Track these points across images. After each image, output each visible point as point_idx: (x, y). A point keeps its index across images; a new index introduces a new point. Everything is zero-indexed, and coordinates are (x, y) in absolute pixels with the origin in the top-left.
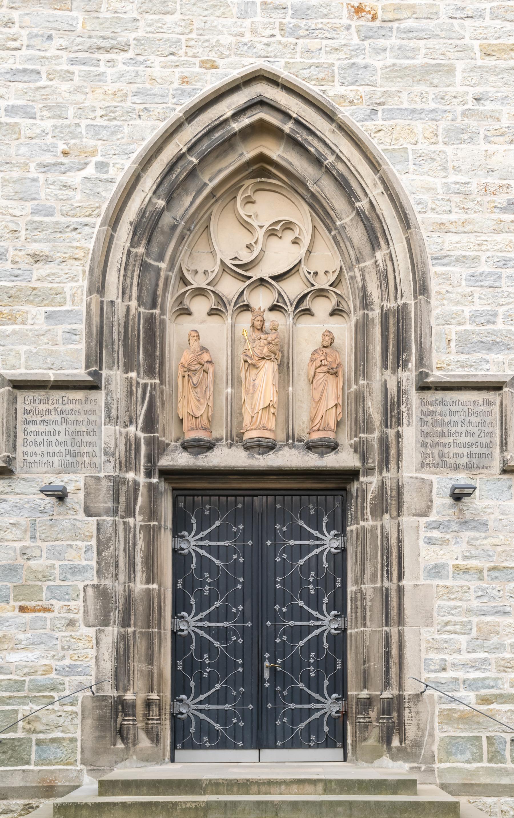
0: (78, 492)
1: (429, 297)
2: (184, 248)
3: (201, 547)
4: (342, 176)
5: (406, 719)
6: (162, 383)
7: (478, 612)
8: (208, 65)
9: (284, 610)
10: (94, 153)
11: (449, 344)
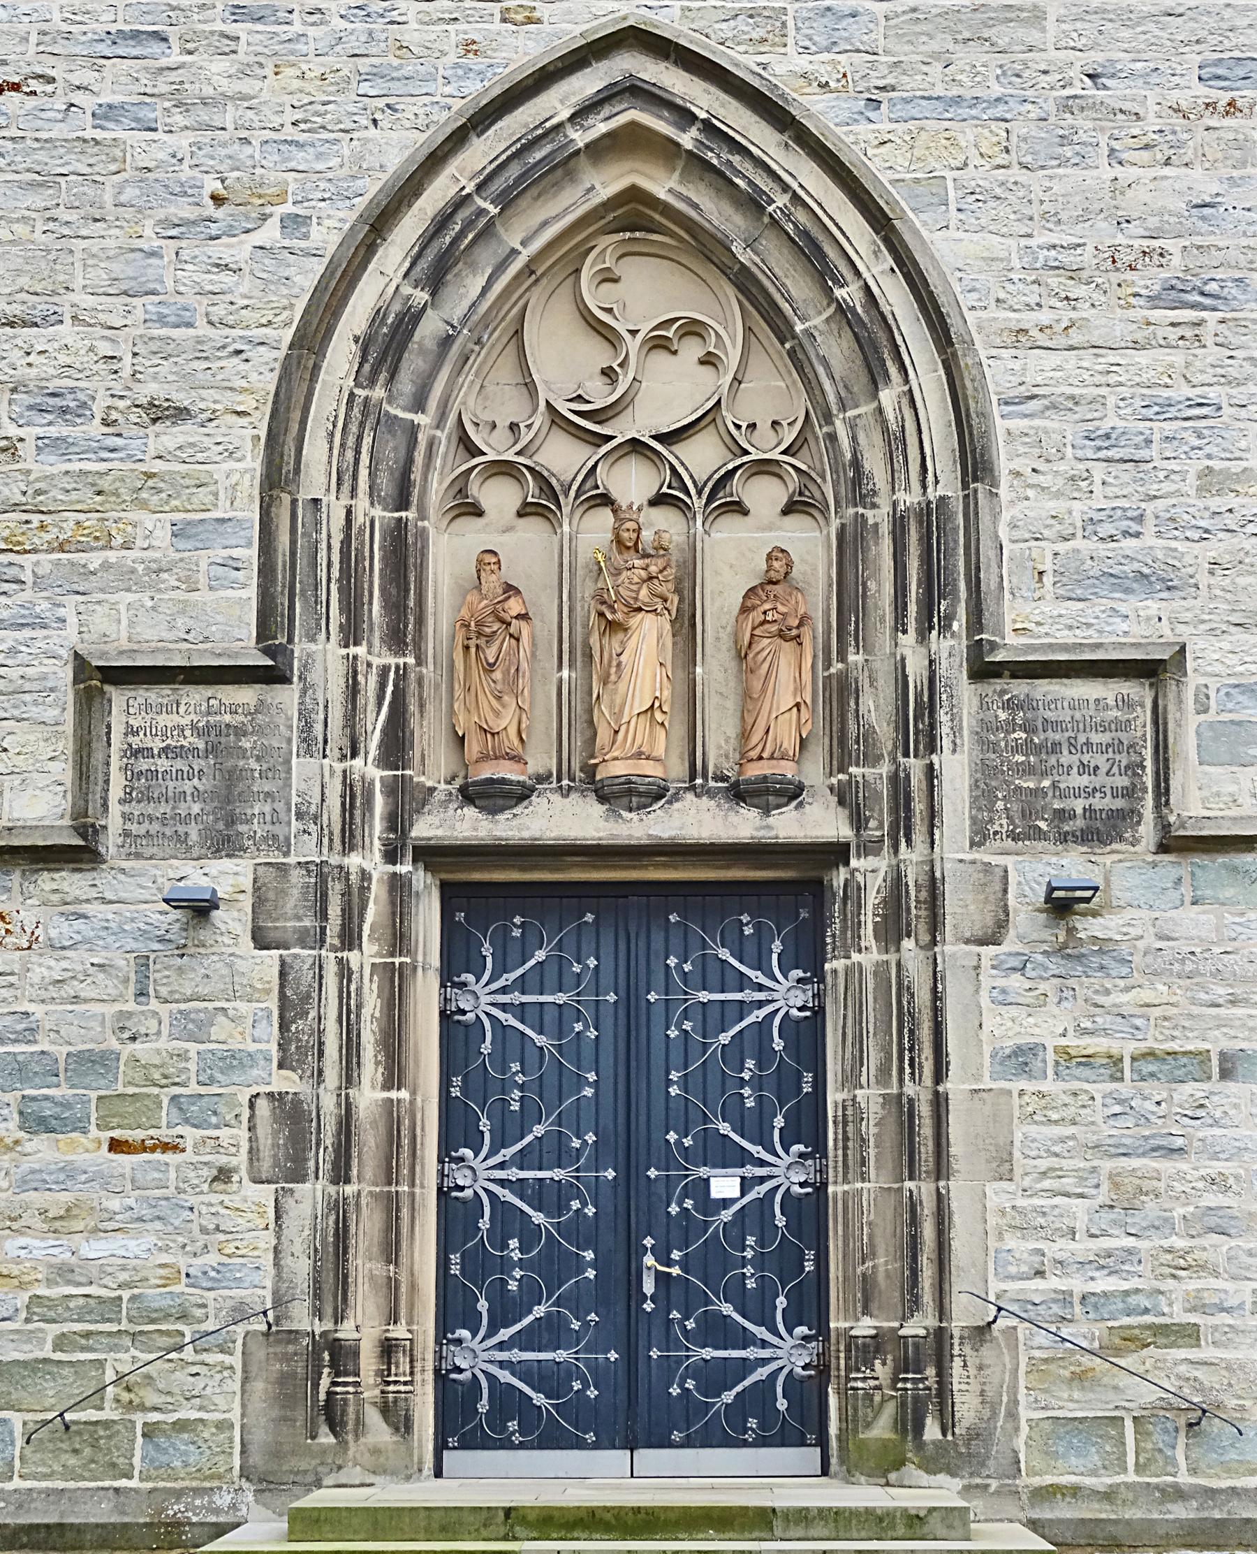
0: (241, 897)
1: (995, 483)
2: (468, 377)
3: (504, 1007)
4: (805, 234)
5: (955, 1380)
6: (419, 662)
7: (1113, 1150)
8: (519, 18)
9: (688, 1142)
10: (281, 197)
11: (1040, 580)
